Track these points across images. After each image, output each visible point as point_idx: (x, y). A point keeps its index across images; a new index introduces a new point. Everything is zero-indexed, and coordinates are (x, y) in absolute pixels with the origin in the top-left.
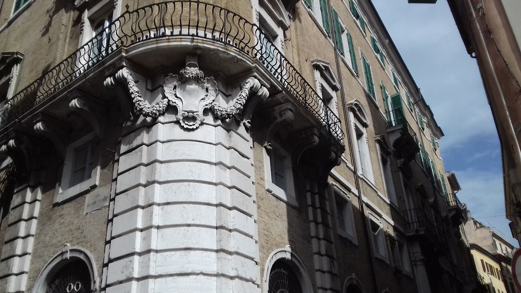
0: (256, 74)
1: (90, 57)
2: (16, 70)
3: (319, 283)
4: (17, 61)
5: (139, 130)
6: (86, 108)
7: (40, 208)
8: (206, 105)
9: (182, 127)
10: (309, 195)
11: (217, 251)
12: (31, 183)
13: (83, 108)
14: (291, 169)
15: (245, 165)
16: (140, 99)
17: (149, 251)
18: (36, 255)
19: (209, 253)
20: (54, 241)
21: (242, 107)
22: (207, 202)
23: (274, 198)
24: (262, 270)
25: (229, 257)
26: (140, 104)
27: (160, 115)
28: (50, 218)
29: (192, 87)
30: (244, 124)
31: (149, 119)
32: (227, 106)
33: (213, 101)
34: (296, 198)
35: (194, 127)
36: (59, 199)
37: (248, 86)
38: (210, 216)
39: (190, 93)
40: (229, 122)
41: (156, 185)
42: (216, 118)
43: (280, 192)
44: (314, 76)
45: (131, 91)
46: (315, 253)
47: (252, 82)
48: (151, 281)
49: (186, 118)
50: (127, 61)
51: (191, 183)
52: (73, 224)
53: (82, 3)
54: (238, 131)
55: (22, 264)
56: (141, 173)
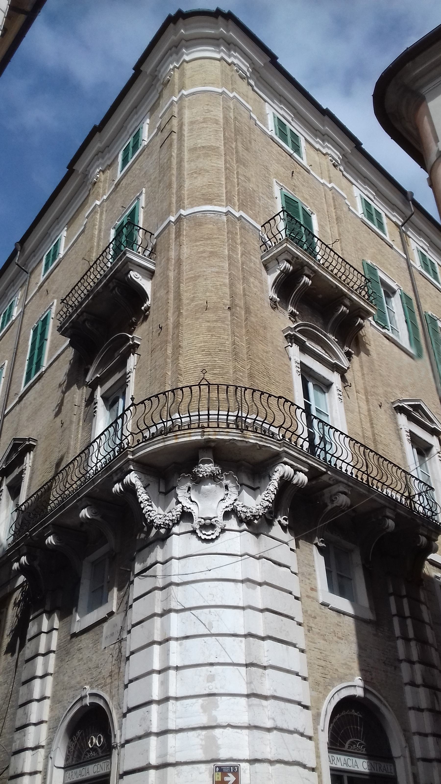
0: (285, 459)
1: (97, 459)
2: (29, 459)
3: (414, 727)
4: (30, 448)
5: (153, 545)
6: (98, 518)
7: (59, 639)
8: (227, 507)
9: (200, 538)
10: (392, 599)
11: (248, 696)
12: (47, 607)
13: (95, 518)
14: (361, 566)
15: (281, 577)
16: (150, 508)
17: (167, 699)
18: (56, 699)
19: (238, 698)
20: (73, 682)
21: (270, 505)
22: (232, 633)
23: (334, 614)
24: (316, 718)
25: (264, 702)
26: (151, 514)
27: (174, 525)
28: (68, 653)
29: (209, 487)
30: (279, 522)
31: (163, 531)
32: (253, 503)
33: (235, 500)
34: (371, 608)
35: (214, 537)
36: (76, 628)
37: (276, 476)
38: (238, 650)
39: (206, 495)
40: (257, 525)
41: (173, 615)
42: (240, 521)
43: (344, 604)
44: (396, 423)
45: (140, 500)
46: (406, 684)
47: (282, 470)
48: (170, 736)
49: (204, 527)
50: (135, 463)
51: (212, 610)
52: (91, 660)
53: (93, 379)
54: (271, 534)
55: (41, 711)
56: (156, 600)
